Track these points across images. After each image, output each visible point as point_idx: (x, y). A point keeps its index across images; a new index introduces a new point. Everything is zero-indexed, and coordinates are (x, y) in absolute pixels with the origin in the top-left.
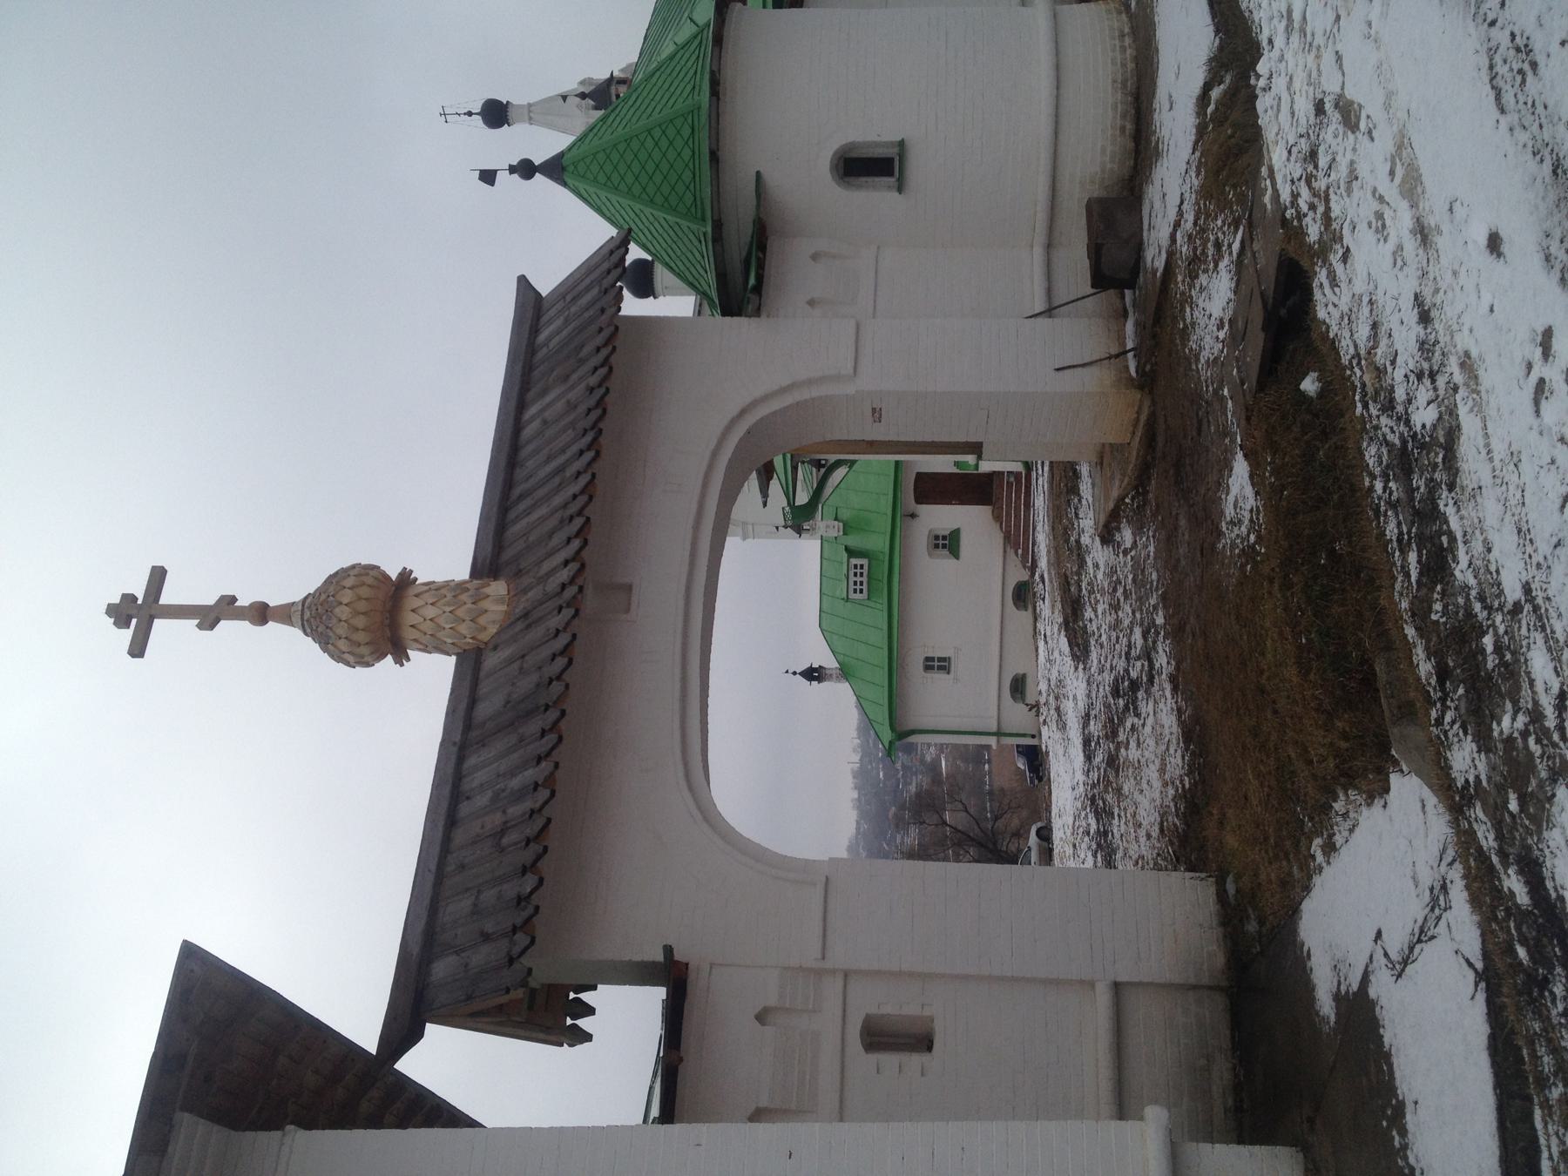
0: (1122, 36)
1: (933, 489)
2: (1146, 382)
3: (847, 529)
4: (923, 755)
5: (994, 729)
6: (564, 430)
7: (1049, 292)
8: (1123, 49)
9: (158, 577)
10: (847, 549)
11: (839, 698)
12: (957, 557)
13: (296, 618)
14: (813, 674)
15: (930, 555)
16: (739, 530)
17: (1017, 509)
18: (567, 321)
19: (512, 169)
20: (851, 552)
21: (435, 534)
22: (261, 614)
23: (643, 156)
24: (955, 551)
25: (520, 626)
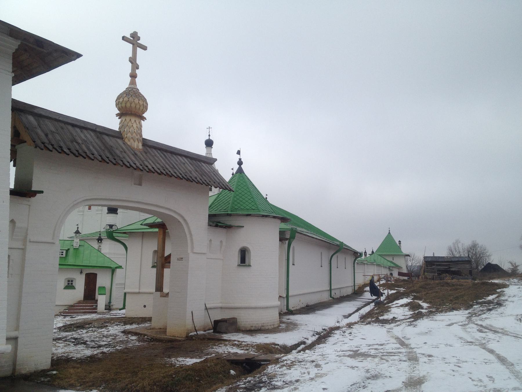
0: (274, 325)
1: (91, 280)
2: (189, 338)
3: (76, 249)
6: (184, 169)
7: (211, 309)
8: (271, 325)
9: (144, 48)
10: (69, 249)
12: (65, 288)
13: (132, 86)
15: (66, 279)
18: (209, 172)
19: (240, 159)
20: (67, 251)
21: (155, 128)
22: (133, 76)
23: (246, 195)
24: (66, 288)
25: (133, 152)
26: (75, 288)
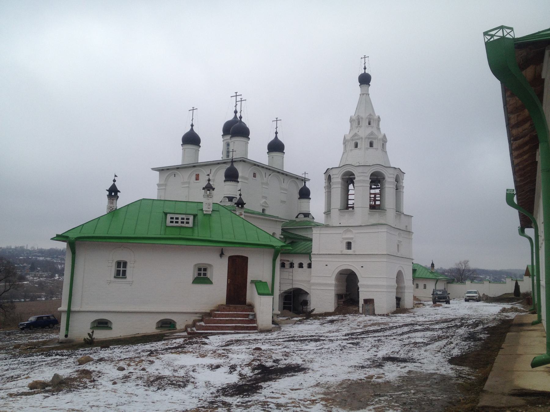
4: (29, 274)
5: (73, 309)
11: (100, 206)
14: (113, 192)
15: (195, 265)
16: (162, 182)
17: (232, 322)
26: (211, 283)
